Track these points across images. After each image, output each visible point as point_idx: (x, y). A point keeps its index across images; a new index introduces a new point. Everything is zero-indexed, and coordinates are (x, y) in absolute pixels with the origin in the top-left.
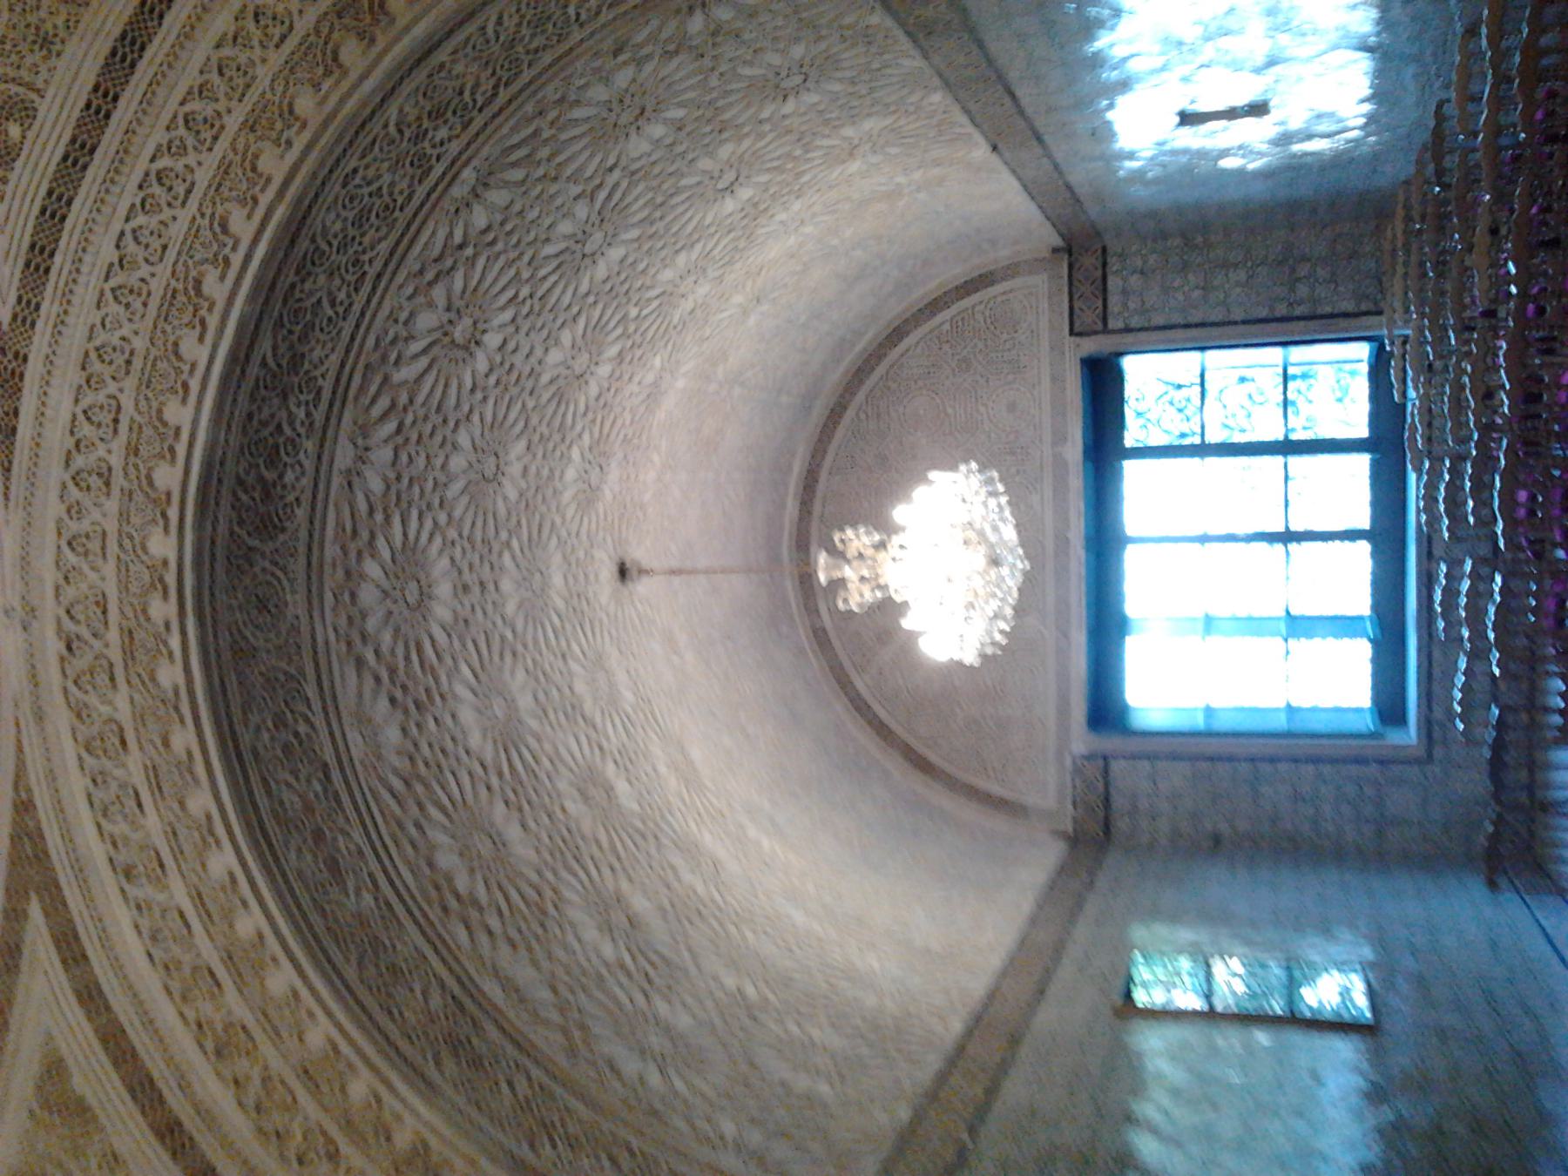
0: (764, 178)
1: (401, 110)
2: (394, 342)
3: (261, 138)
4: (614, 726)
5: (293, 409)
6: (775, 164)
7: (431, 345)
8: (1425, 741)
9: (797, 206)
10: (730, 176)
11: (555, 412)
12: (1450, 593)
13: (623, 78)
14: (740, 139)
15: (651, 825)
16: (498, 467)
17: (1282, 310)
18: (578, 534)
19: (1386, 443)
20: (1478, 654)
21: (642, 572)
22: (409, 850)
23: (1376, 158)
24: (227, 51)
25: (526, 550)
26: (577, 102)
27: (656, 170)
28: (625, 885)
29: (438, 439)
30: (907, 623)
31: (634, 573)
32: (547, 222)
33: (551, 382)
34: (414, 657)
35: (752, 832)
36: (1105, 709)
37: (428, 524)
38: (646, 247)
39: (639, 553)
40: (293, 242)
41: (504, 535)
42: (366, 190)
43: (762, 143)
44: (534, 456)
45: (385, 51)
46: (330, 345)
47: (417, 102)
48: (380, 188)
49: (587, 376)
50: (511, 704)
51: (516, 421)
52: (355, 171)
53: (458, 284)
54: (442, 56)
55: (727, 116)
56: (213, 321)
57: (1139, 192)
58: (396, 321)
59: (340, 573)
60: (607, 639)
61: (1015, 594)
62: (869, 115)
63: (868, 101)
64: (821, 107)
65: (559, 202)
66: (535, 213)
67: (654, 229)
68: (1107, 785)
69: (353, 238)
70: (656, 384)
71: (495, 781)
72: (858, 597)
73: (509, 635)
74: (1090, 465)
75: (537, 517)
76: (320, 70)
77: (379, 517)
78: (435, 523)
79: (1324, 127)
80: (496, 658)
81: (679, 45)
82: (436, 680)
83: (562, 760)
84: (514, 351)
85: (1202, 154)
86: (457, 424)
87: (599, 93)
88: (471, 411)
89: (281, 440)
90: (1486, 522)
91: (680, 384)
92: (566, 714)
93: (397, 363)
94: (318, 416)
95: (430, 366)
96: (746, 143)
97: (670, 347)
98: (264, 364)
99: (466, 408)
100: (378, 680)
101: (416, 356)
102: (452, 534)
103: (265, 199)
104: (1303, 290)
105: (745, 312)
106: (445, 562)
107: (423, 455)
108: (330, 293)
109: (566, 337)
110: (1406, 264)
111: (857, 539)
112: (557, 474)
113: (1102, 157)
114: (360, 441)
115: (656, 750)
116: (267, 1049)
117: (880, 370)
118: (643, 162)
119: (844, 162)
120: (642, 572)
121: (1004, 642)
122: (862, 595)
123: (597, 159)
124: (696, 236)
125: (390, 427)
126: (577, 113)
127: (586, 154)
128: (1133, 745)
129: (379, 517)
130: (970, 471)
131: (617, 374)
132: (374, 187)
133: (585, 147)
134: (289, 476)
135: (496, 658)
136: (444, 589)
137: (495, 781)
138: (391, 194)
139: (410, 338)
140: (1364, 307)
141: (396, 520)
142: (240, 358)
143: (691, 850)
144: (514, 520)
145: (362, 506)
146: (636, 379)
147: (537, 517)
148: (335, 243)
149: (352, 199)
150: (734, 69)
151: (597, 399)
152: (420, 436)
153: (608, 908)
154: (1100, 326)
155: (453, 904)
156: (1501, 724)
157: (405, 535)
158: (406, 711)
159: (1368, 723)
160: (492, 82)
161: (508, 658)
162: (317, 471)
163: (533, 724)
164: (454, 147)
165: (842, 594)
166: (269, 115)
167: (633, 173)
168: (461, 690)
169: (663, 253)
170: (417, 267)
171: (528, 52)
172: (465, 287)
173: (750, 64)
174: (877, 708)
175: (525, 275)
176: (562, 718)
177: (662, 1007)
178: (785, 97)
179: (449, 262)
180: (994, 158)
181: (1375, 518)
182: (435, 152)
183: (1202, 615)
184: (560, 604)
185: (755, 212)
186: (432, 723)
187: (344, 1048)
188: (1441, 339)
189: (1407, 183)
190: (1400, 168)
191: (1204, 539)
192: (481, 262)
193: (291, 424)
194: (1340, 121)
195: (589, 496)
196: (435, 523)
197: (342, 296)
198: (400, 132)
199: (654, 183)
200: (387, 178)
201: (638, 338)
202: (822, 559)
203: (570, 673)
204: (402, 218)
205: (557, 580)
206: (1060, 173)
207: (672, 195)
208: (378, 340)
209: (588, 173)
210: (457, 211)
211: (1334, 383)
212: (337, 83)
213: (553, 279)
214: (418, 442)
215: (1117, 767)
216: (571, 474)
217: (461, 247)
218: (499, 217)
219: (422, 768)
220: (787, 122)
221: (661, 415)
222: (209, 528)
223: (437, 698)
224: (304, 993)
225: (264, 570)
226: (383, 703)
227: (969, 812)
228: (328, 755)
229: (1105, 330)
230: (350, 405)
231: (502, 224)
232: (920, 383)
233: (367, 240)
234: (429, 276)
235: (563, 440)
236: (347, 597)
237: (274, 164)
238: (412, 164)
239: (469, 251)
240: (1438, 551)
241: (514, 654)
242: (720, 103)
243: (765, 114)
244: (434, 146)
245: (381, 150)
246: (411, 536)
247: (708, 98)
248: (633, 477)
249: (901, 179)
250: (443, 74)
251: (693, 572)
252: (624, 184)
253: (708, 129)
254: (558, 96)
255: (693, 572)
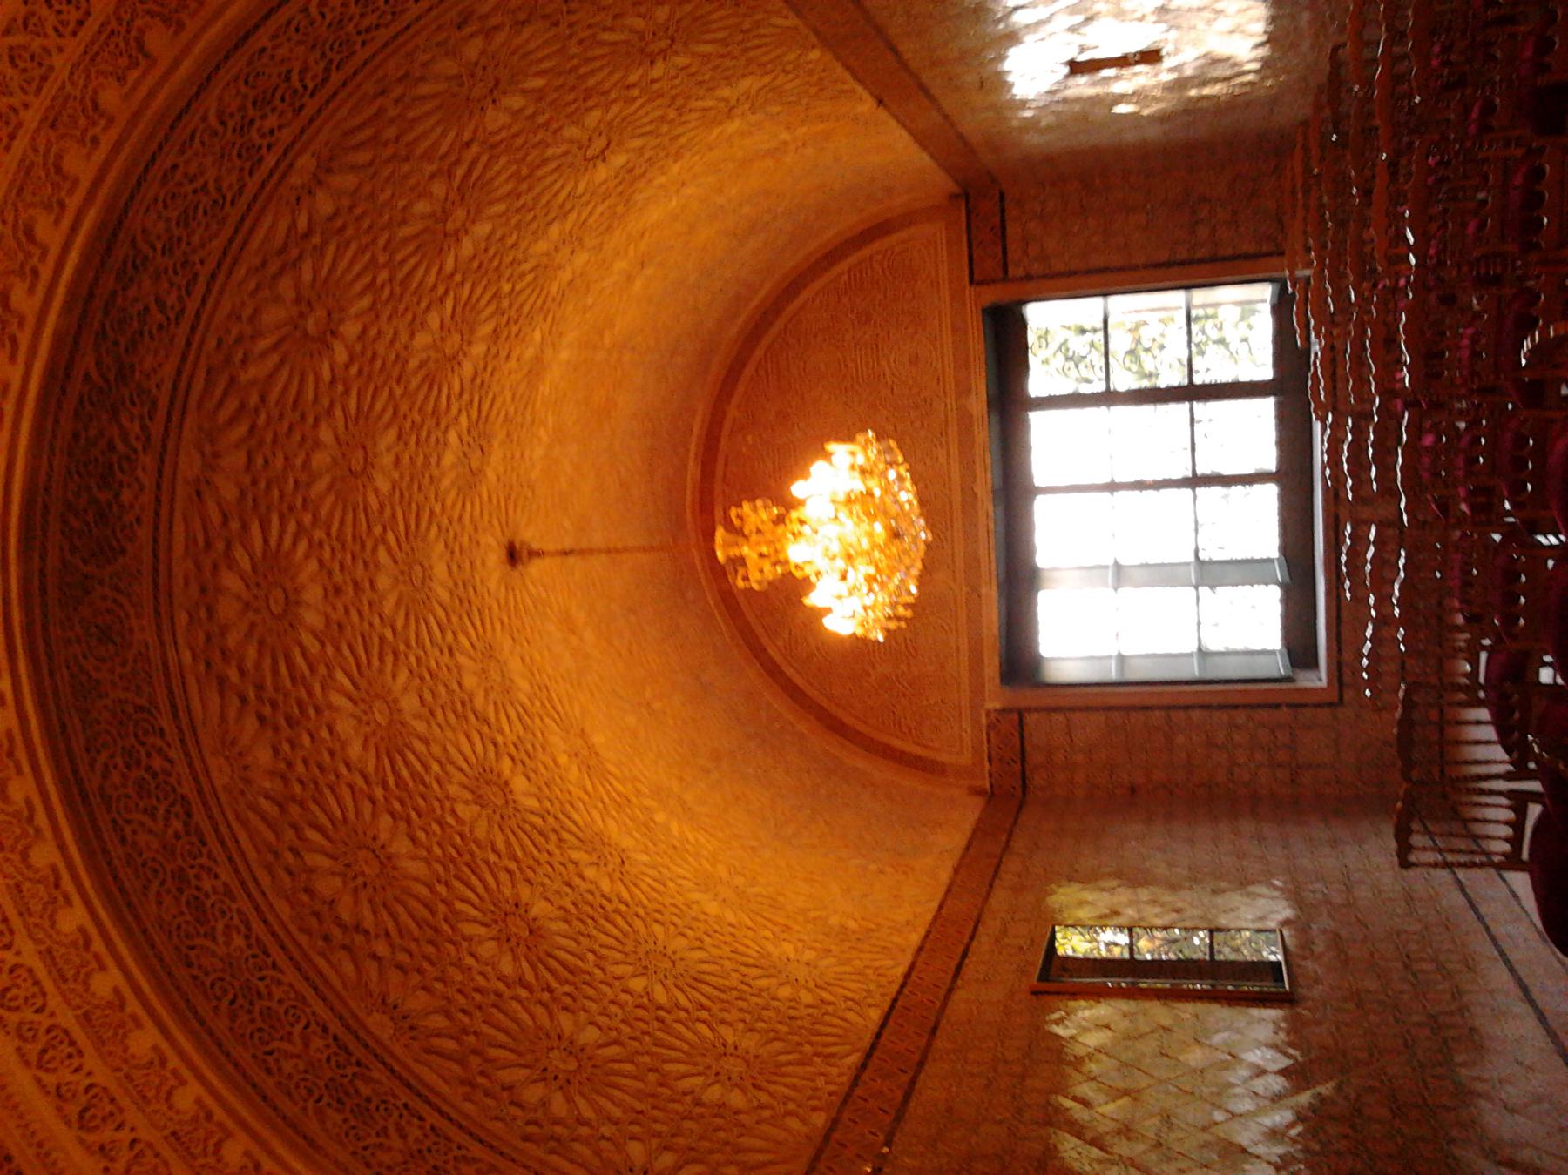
0: (637, 143)
1: (220, 99)
2: (240, 339)
3: (62, 137)
4: (508, 717)
5: (125, 423)
6: (648, 128)
7: (282, 340)
8: (1336, 685)
9: (676, 168)
10: (600, 143)
11: (427, 397)
12: (1356, 554)
13: (472, 50)
14: (607, 106)
15: (551, 820)
16: (366, 460)
17: (1183, 254)
18: (460, 518)
19: (1289, 386)
20: (1383, 621)
21: (534, 554)
22: (286, 878)
23: (1274, 101)
24: (18, 39)
25: (403, 544)
26: (422, 79)
27: (519, 141)
28: (525, 893)
29: (297, 437)
30: (813, 599)
31: (525, 554)
32: (401, 203)
33: (420, 367)
34: (283, 670)
35: (660, 817)
36: (1018, 660)
37: (292, 527)
38: (514, 221)
39: (530, 535)
40: (109, 249)
41: (378, 530)
42: (189, 188)
43: (633, 108)
44: (406, 444)
45: (196, 37)
46: (162, 353)
47: (238, 92)
48: (206, 184)
49: (461, 357)
50: (393, 707)
51: (383, 411)
52: (175, 167)
53: (307, 276)
54: (263, 38)
55: (591, 82)
56: (24, 340)
57: (1034, 140)
58: (239, 318)
59: (194, 590)
60: (498, 626)
61: (919, 565)
62: (743, 76)
63: (742, 61)
64: (693, 70)
65: (412, 181)
66: (388, 193)
67: (521, 201)
68: (1022, 738)
69: (179, 240)
70: (538, 359)
71: (379, 792)
72: (758, 574)
73: (389, 634)
74: (995, 418)
75: (414, 506)
76: (124, 61)
77: (235, 525)
78: (299, 524)
79: (1219, 72)
80: (376, 662)
81: (530, 14)
82: (310, 693)
83: (452, 763)
84: (375, 340)
85: (1095, 100)
86: (317, 420)
87: (448, 66)
88: (332, 405)
89: (115, 459)
90: (1389, 492)
91: (564, 355)
92: (455, 713)
93: (244, 362)
94: (156, 429)
95: (282, 362)
96: (615, 109)
97: (549, 319)
98: (87, 377)
99: (326, 402)
100: (243, 699)
101: (264, 355)
102: (319, 534)
103: (73, 203)
104: (1203, 232)
105: (630, 278)
106: (313, 566)
107: (280, 456)
108: (158, 300)
109: (433, 320)
110: (1306, 207)
111: (755, 514)
112: (433, 460)
113: (993, 107)
114: (208, 449)
115: (556, 740)
116: (132, 1116)
117: (779, 325)
118: (504, 134)
119: (721, 123)
120: (534, 554)
121: (909, 614)
122: (761, 571)
123: (452, 135)
124: (568, 206)
125: (241, 430)
126: (425, 89)
127: (439, 130)
128: (1047, 700)
129: (235, 525)
130: (867, 441)
131: (494, 350)
132: (198, 184)
133: (438, 123)
134: (127, 495)
135: (376, 662)
136: (313, 594)
137: (379, 792)
138: (219, 190)
139: (257, 335)
140: (1265, 249)
141: (255, 528)
142: (58, 376)
143: (596, 844)
144: (388, 511)
145: (215, 516)
146: (514, 355)
147: (414, 506)
148: (159, 246)
149: (173, 196)
150: (594, 36)
151: (474, 379)
152: (275, 435)
153: (507, 918)
154: (1001, 275)
155: (337, 932)
156: (1408, 703)
157: (266, 541)
158: (276, 729)
159: (1280, 667)
160: (322, 65)
161: (389, 659)
162: (159, 486)
163: (420, 727)
164: (286, 135)
165: (741, 572)
166: (70, 111)
167: (493, 147)
168: (339, 700)
169: (535, 225)
170: (257, 261)
171: (359, 33)
172: (314, 280)
173: (611, 29)
174: (789, 672)
175: (382, 259)
176: (451, 716)
177: (565, 1021)
178: (652, 63)
179: (294, 253)
180: (882, 114)
181: (1281, 460)
182: (265, 143)
183: (1111, 563)
184: (444, 596)
185: (631, 176)
186: (306, 740)
187: (219, 1114)
188: (1340, 294)
189: (1304, 123)
190: (1297, 109)
191: (1112, 487)
192: (331, 249)
193: (125, 440)
194: (1236, 65)
195: (472, 478)
196: (299, 524)
197: (171, 300)
198: (223, 123)
199: (519, 155)
200: (211, 175)
201: (513, 313)
202: (720, 534)
203: (458, 666)
204: (234, 214)
205: (440, 570)
206: (952, 125)
207: (539, 167)
208: (220, 342)
209: (443, 149)
210: (298, 199)
211: (1238, 326)
212: (144, 74)
213: (412, 261)
214: (274, 441)
215: (1031, 719)
216: (449, 459)
217: (307, 235)
218: (346, 202)
219: (298, 789)
220: (656, 86)
221: (545, 388)
222: (37, 558)
223: (312, 712)
224: (169, 1052)
225: (104, 598)
226: (251, 723)
227: (882, 772)
228: (187, 788)
229: (1005, 277)
230: (190, 421)
231: (351, 208)
232: (820, 337)
233: (196, 239)
234: (273, 268)
235: (438, 424)
236: (203, 614)
237: (80, 165)
238: (239, 155)
239: (316, 240)
240: (1343, 512)
241: (396, 654)
242: (582, 71)
243: (633, 78)
244: (263, 136)
245: (203, 143)
246: (273, 542)
247: (569, 66)
248: (518, 455)
249: (785, 136)
250: (265, 60)
251: (591, 551)
252: (485, 158)
253: (572, 97)
254: (401, 73)
255: (591, 551)
